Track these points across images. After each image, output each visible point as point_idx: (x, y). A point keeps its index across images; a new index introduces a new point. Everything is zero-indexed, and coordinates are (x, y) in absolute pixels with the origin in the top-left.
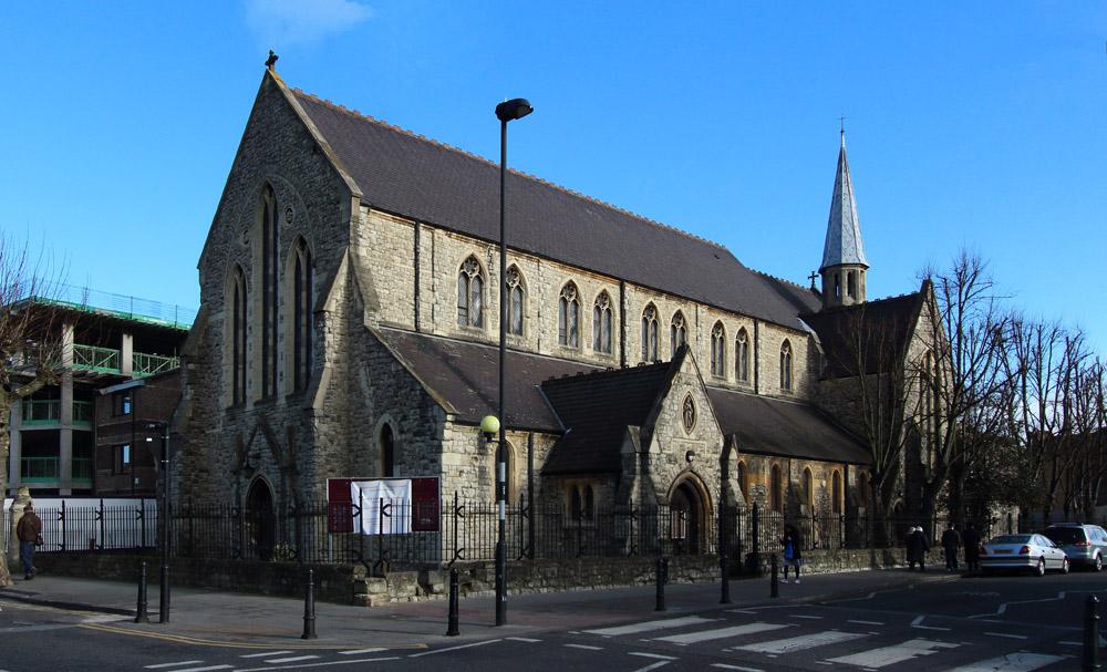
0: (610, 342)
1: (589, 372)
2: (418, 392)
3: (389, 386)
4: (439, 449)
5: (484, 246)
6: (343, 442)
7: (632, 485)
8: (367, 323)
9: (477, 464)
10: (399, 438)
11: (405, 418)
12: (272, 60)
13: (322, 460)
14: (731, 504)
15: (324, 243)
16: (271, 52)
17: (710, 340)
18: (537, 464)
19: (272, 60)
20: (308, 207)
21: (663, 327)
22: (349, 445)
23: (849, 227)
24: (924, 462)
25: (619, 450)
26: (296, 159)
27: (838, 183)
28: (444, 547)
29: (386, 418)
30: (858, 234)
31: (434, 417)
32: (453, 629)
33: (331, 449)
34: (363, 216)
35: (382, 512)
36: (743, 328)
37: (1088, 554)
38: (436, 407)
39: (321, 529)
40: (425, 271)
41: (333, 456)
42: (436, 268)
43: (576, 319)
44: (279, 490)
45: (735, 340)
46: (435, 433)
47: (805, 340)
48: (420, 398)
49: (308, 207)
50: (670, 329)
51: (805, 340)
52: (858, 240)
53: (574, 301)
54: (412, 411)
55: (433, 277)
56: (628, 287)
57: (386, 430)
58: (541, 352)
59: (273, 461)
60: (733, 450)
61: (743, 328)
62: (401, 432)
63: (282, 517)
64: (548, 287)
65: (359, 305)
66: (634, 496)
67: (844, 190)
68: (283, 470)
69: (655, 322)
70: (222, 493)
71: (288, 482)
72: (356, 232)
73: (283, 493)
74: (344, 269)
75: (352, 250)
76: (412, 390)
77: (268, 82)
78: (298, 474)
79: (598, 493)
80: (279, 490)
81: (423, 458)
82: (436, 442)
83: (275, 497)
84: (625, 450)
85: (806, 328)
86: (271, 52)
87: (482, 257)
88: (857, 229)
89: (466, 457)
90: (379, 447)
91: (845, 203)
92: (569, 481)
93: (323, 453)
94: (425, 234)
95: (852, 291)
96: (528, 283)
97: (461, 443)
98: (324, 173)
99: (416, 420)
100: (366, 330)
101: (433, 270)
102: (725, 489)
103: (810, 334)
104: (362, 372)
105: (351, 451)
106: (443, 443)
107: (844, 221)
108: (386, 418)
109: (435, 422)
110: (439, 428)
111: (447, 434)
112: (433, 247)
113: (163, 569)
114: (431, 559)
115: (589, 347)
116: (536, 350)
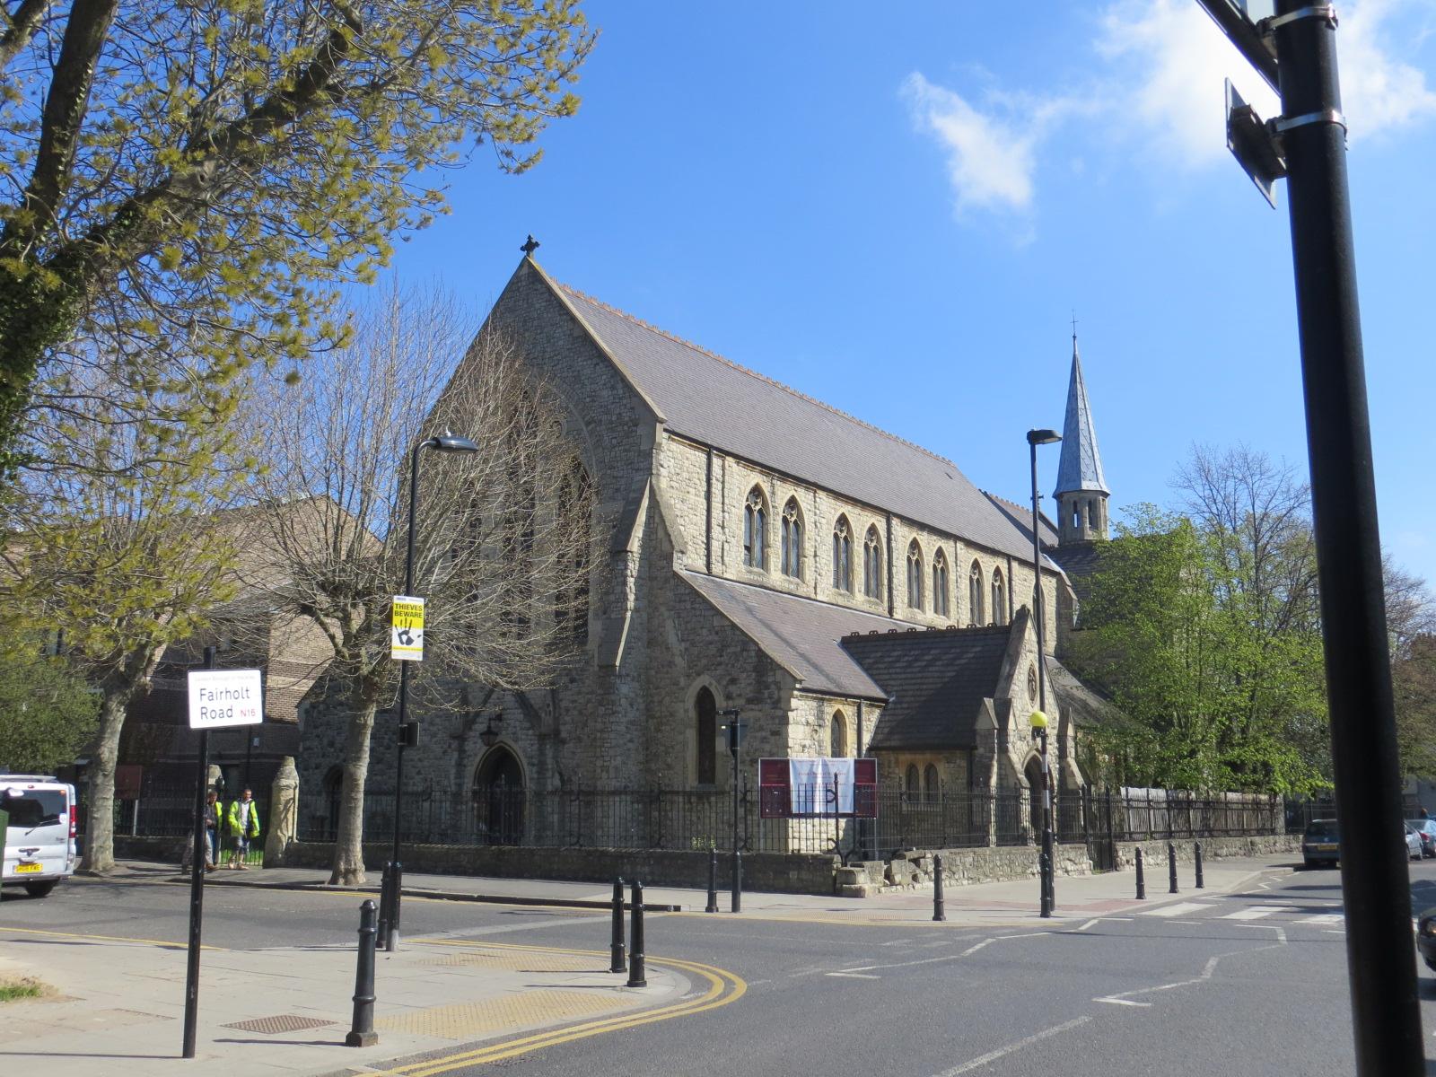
0: (877, 585)
1: (905, 630)
2: (753, 654)
3: (711, 643)
4: (785, 721)
5: (767, 475)
6: (642, 706)
7: (991, 765)
8: (677, 567)
9: (816, 737)
10: (724, 704)
11: (733, 681)
12: (530, 246)
13: (622, 728)
14: (1071, 786)
15: (612, 468)
16: (530, 237)
17: (968, 582)
18: (867, 738)
19: (530, 246)
20: (588, 424)
21: (926, 567)
22: (648, 709)
23: (1087, 448)
24: (954, 674)
25: (973, 724)
26: (571, 367)
27: (1073, 396)
28: (791, 836)
29: (704, 680)
30: (1097, 456)
31: (776, 683)
32: (938, 915)
33: (632, 715)
34: (664, 441)
35: (836, 794)
36: (793, 497)
37: (476, 805)
38: (779, 673)
39: (617, 813)
40: (716, 505)
41: (632, 723)
42: (726, 501)
43: (847, 557)
44: (535, 761)
45: (906, 554)
46: (779, 701)
47: (1054, 580)
48: (755, 660)
49: (588, 424)
50: (931, 570)
51: (1054, 580)
52: (1098, 463)
53: (795, 521)
54: (744, 675)
55: (723, 511)
56: (895, 521)
57: (705, 697)
58: (819, 598)
59: (528, 725)
60: (1070, 725)
61: (793, 497)
62: (729, 697)
63: (539, 795)
64: (824, 521)
65: (666, 547)
66: (994, 781)
67: (1080, 405)
68: (542, 738)
69: (942, 569)
70: (426, 763)
71: (549, 753)
72: (658, 460)
73: (541, 767)
74: (645, 503)
75: (654, 482)
76: (743, 650)
77: (525, 270)
78: (563, 742)
79: (943, 772)
80: (535, 761)
81: (761, 729)
82: (779, 713)
83: (528, 772)
84: (981, 725)
85: (1056, 568)
86: (530, 237)
87: (766, 488)
88: (1095, 449)
89: (808, 729)
90: (693, 714)
91: (1082, 419)
92: (906, 758)
93: (624, 720)
94: (716, 462)
95: (1095, 524)
96: (806, 517)
97: (803, 713)
98: (613, 388)
99: (749, 684)
100: (676, 575)
101: (723, 503)
102: (1064, 770)
103: (1059, 574)
104: (669, 625)
105: (653, 717)
106: (790, 714)
107: (1082, 441)
108: (704, 680)
109: (779, 689)
110: (783, 694)
111: (794, 703)
112: (723, 476)
113: (712, 865)
114: (685, 848)
115: (860, 591)
116: (813, 596)
